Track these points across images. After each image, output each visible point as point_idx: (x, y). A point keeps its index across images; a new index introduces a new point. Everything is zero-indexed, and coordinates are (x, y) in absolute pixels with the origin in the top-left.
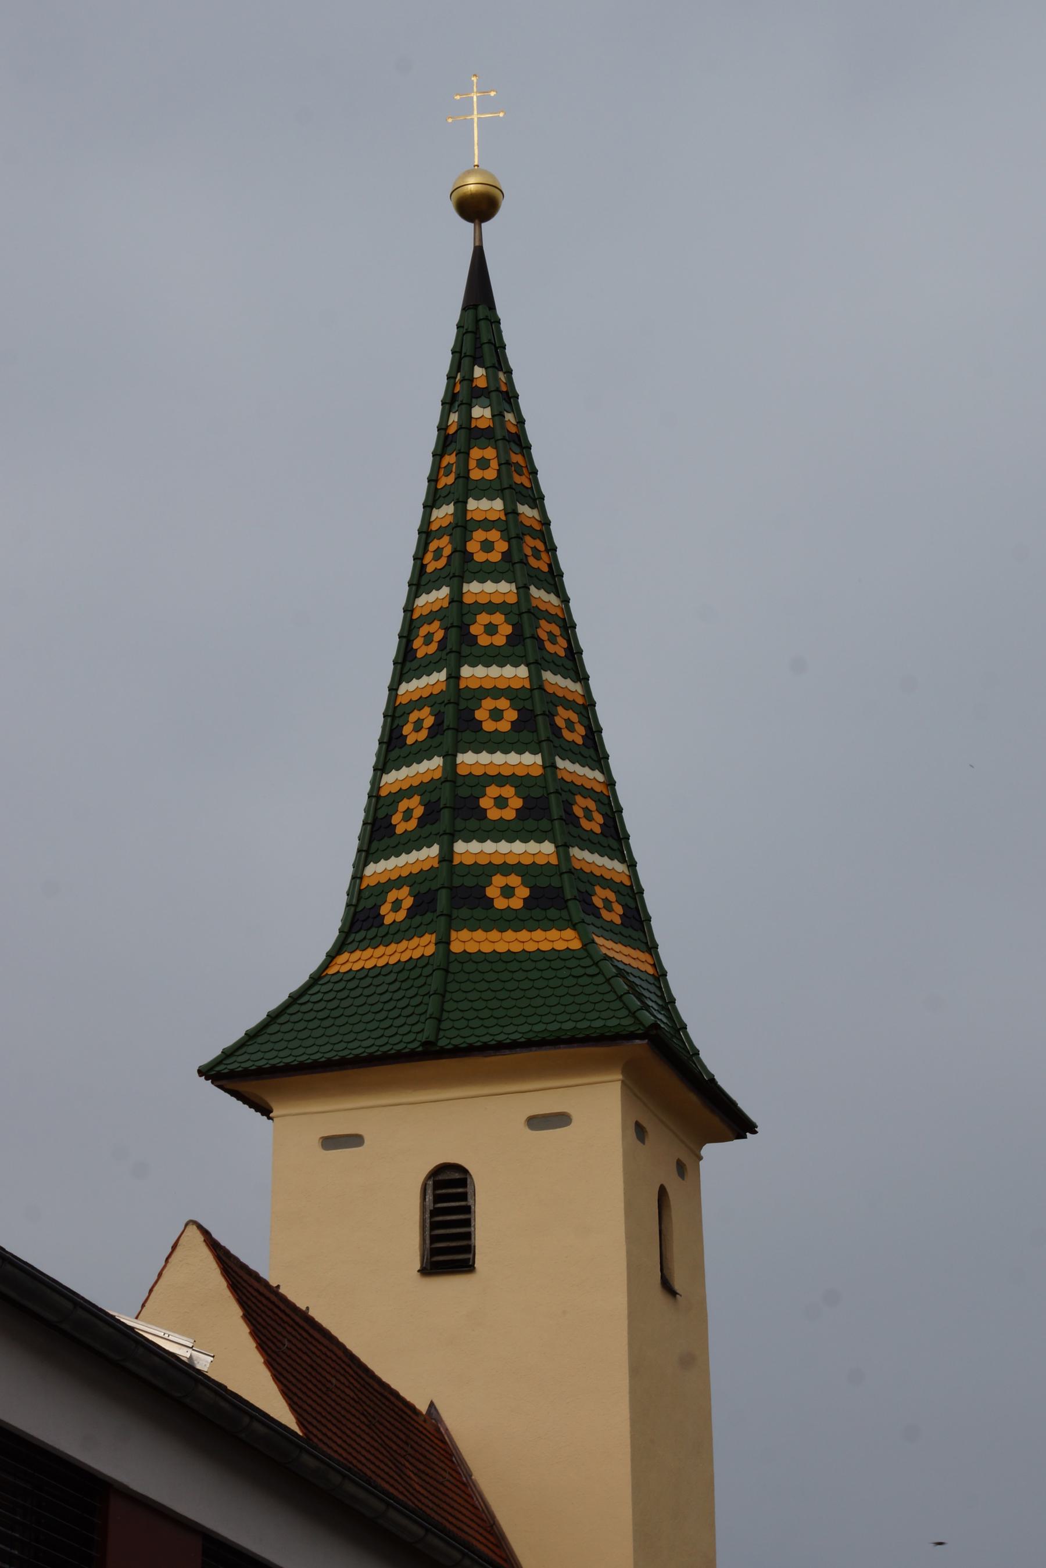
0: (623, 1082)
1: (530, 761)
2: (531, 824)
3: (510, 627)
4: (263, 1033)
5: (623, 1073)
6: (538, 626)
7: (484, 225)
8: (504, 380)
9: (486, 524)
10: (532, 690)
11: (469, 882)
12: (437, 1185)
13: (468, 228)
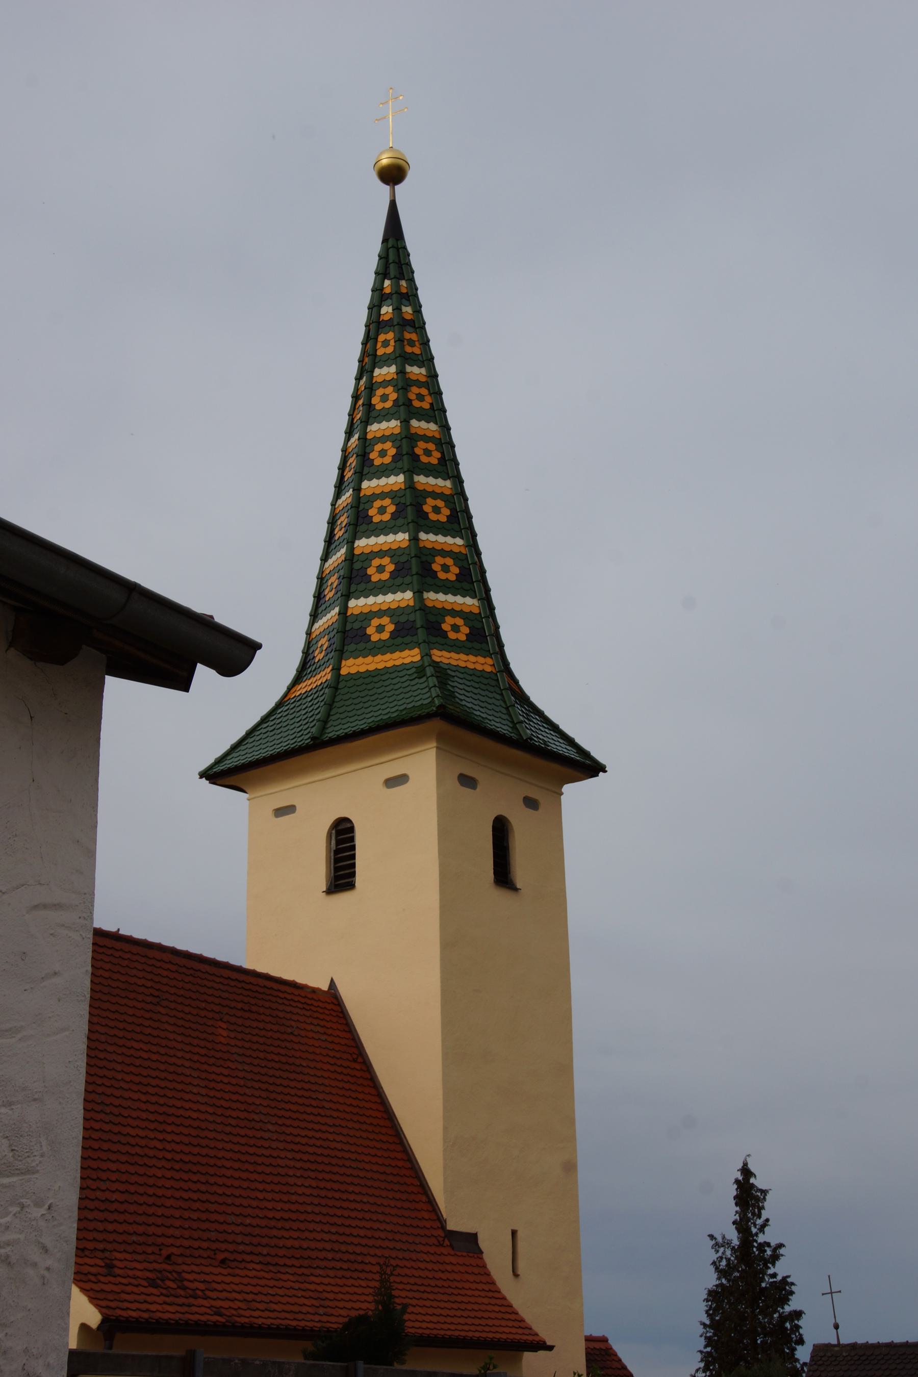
0: (437, 748)
1: (402, 537)
2: (399, 581)
3: (395, 449)
4: (245, 743)
5: (437, 742)
6: (417, 446)
7: (396, 187)
8: (405, 285)
9: (385, 383)
10: (405, 489)
11: (356, 626)
12: (338, 833)
13: (387, 188)
